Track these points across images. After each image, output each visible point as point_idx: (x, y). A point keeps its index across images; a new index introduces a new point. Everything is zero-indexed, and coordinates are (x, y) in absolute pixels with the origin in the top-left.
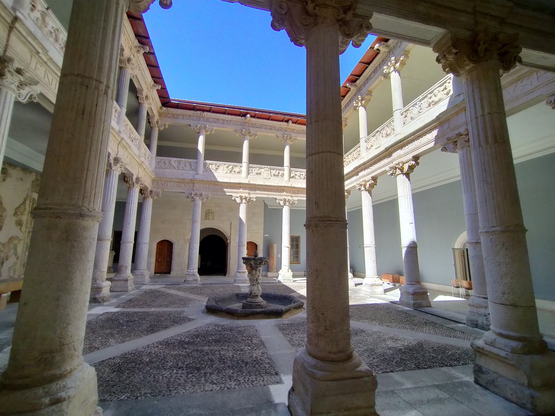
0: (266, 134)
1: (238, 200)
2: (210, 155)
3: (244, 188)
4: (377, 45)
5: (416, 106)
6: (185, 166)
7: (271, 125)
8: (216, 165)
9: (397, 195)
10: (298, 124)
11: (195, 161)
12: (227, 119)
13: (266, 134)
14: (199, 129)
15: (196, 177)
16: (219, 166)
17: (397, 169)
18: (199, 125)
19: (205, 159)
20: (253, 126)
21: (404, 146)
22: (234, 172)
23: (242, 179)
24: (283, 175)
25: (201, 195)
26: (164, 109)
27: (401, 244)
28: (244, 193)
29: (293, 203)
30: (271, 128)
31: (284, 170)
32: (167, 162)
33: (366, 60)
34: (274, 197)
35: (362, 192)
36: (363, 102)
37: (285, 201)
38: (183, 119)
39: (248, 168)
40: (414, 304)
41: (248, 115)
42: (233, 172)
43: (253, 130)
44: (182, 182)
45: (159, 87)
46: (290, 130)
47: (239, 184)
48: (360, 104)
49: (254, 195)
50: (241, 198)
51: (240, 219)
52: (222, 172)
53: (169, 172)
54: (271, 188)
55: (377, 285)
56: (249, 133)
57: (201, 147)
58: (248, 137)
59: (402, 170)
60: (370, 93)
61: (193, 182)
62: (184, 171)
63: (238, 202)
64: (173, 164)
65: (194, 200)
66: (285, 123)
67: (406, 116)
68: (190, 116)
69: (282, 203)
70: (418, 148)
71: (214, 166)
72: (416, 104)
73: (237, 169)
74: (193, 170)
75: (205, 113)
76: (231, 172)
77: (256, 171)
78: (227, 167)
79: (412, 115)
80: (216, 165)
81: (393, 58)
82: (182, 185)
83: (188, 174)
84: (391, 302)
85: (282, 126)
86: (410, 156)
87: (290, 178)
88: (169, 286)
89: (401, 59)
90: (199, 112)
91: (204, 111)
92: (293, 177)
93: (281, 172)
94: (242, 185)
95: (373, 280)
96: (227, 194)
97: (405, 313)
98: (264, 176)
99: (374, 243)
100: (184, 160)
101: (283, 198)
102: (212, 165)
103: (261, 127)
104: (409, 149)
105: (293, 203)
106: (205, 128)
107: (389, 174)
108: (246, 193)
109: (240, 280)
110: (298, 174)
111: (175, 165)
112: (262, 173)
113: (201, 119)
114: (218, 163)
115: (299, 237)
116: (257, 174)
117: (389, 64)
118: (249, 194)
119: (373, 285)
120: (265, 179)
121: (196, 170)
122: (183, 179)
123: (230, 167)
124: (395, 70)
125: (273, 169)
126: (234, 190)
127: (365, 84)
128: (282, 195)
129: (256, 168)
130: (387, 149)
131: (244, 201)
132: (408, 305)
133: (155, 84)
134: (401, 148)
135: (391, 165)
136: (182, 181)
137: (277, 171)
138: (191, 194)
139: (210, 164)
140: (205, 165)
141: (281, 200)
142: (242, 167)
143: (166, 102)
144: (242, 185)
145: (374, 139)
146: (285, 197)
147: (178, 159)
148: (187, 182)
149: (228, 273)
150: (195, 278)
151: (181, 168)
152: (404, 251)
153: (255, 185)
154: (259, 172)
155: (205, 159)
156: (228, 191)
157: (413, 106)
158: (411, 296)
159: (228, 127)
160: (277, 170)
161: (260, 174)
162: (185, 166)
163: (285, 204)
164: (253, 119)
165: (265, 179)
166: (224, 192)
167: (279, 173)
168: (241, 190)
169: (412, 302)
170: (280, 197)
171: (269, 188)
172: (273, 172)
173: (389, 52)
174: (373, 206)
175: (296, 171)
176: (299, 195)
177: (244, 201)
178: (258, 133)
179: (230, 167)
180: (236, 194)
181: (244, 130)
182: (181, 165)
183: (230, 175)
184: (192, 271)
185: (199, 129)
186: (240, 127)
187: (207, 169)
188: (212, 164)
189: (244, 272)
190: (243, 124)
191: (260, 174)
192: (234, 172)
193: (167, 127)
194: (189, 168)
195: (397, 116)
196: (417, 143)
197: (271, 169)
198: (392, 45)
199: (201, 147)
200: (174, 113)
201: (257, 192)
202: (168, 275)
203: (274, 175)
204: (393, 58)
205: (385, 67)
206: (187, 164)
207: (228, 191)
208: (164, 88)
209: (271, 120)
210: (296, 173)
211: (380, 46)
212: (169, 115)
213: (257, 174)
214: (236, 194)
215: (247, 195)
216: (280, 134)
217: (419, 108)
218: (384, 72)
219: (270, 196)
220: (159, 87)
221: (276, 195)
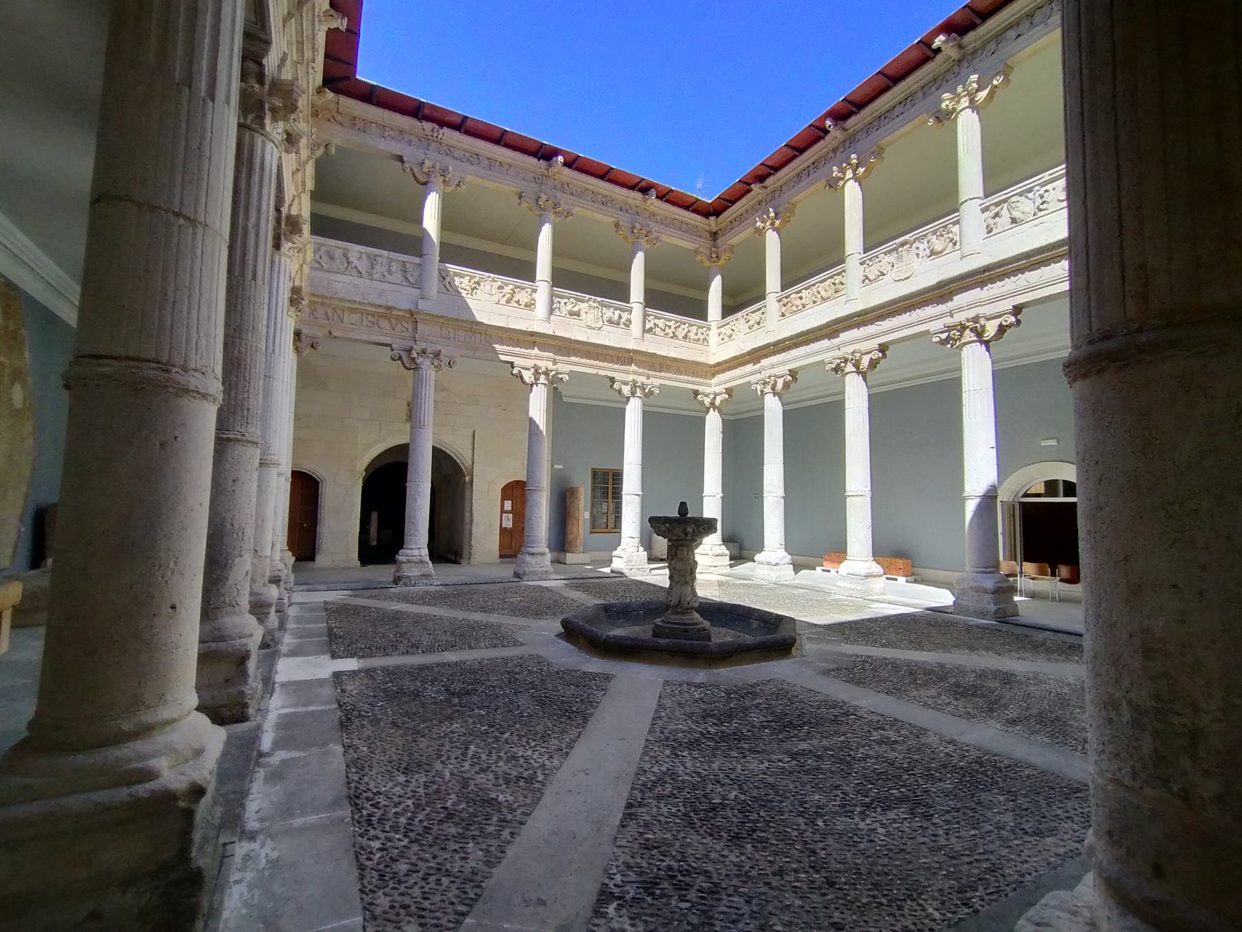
0: (589, 214)
1: (528, 376)
2: (451, 253)
3: (543, 348)
4: (942, 38)
5: (1030, 195)
6: (390, 272)
7: (606, 193)
8: (472, 278)
9: (843, 393)
10: (667, 201)
11: (417, 260)
12: (500, 159)
13: (589, 214)
14: (428, 174)
15: (422, 305)
16: (478, 283)
17: (967, 332)
18: (428, 163)
19: (443, 260)
20: (564, 187)
21: (992, 281)
22: (518, 302)
23: (537, 321)
24: (628, 323)
25: (437, 355)
26: (330, 95)
27: (963, 490)
28: (544, 360)
29: (651, 393)
30: (605, 202)
31: (630, 311)
32: (338, 254)
33: (890, 72)
34: (610, 374)
35: (848, 378)
36: (861, 170)
37: (635, 385)
38: (385, 136)
39: (552, 296)
40: (996, 613)
41: (560, 159)
42: (513, 303)
43: (564, 200)
44: (384, 316)
45: (341, 24)
46: (647, 215)
47: (532, 334)
48: (849, 174)
49: (566, 366)
50: (537, 373)
51: (532, 421)
52: (487, 299)
53: (343, 284)
54: (606, 352)
55: (874, 576)
56: (556, 205)
57: (431, 221)
58: (552, 216)
59: (979, 333)
60: (879, 153)
61: (413, 316)
62: (386, 286)
63: (527, 379)
64: (356, 263)
65: (417, 368)
66: (639, 195)
67: (997, 215)
68: (401, 132)
69: (626, 390)
70: (1034, 289)
71: (465, 281)
72: (1030, 190)
73: (523, 297)
74: (412, 285)
75: (445, 130)
76: (508, 301)
77: (569, 307)
78: (500, 288)
79: (1016, 214)
80: (472, 278)
81: (974, 77)
82: (384, 323)
83: (402, 298)
84: (928, 609)
85: (631, 201)
86: (1008, 305)
87: (644, 331)
88: (359, 593)
89: (995, 82)
90: (428, 126)
91: (442, 124)
92: (651, 329)
93: (625, 316)
94: (538, 340)
95: (867, 565)
96: (502, 358)
97: (984, 628)
98: (587, 320)
99: (869, 488)
100: (385, 253)
101: (631, 377)
102: (463, 278)
103: (582, 194)
104: (1005, 289)
105: (651, 393)
106: (444, 173)
107: (935, 339)
108: (548, 359)
109: (535, 573)
110: (661, 323)
111: (363, 265)
112: (582, 314)
113: (433, 145)
114: (479, 274)
115: (595, 473)
116: (572, 314)
117: (960, 89)
118: (555, 362)
119: (867, 576)
120: (590, 328)
121: (419, 285)
122: (389, 308)
123: (508, 289)
124: (973, 105)
125: (608, 307)
126: (517, 350)
127: (868, 128)
128: (627, 372)
129: (569, 300)
130: (941, 285)
131: (542, 379)
132: (982, 614)
133: (332, 12)
134: (982, 284)
135: (949, 321)
136: (387, 312)
137: (617, 313)
138: (410, 351)
139: (456, 274)
140: (443, 276)
141: (626, 383)
142: (535, 291)
143: (340, 76)
144: (538, 340)
145: (892, 258)
146: (635, 377)
147: (370, 250)
148: (397, 318)
149: (465, 554)
150: (425, 571)
151: (375, 277)
152: (970, 507)
153: (569, 340)
154: (576, 309)
155: (443, 260)
156: (505, 352)
157: (1020, 194)
158: (988, 597)
159: (498, 183)
160: (616, 309)
161: (578, 314)
162: (390, 272)
163: (633, 394)
164: (567, 171)
165: (590, 328)
166: (495, 352)
167: (620, 317)
168: (536, 351)
169: (992, 608)
170: (625, 375)
171: (600, 351)
172: (608, 313)
173: (959, 61)
174: (784, 412)
175: (656, 318)
176: (663, 374)
177: (542, 379)
178: (576, 210)
179: (508, 289)
180: (526, 361)
181: (544, 197)
182: (378, 268)
183: (507, 310)
184: (416, 552)
185: (428, 174)
186: (533, 185)
187: (447, 286)
188: (462, 276)
189: (542, 554)
190: (539, 180)
191: (578, 314)
192: (518, 302)
193: (333, 150)
194: (398, 277)
195: (972, 214)
196: (1032, 277)
197: (602, 305)
198: (970, 47)
199: (431, 221)
200: (356, 113)
201: (573, 359)
202: (310, 564)
203: (610, 321)
204: (974, 77)
205: (946, 95)
206: (394, 268)
207: (505, 352)
208: (353, 33)
209: (610, 181)
210: (657, 321)
211: (946, 42)
212: (339, 118)
213: (572, 314)
214: (526, 361)
215: (550, 365)
216: (624, 219)
217: (1039, 201)
218: (943, 105)
219: (602, 373)
220: (341, 24)
221: (615, 370)
